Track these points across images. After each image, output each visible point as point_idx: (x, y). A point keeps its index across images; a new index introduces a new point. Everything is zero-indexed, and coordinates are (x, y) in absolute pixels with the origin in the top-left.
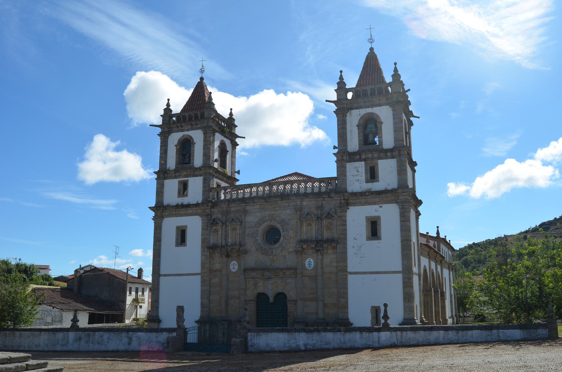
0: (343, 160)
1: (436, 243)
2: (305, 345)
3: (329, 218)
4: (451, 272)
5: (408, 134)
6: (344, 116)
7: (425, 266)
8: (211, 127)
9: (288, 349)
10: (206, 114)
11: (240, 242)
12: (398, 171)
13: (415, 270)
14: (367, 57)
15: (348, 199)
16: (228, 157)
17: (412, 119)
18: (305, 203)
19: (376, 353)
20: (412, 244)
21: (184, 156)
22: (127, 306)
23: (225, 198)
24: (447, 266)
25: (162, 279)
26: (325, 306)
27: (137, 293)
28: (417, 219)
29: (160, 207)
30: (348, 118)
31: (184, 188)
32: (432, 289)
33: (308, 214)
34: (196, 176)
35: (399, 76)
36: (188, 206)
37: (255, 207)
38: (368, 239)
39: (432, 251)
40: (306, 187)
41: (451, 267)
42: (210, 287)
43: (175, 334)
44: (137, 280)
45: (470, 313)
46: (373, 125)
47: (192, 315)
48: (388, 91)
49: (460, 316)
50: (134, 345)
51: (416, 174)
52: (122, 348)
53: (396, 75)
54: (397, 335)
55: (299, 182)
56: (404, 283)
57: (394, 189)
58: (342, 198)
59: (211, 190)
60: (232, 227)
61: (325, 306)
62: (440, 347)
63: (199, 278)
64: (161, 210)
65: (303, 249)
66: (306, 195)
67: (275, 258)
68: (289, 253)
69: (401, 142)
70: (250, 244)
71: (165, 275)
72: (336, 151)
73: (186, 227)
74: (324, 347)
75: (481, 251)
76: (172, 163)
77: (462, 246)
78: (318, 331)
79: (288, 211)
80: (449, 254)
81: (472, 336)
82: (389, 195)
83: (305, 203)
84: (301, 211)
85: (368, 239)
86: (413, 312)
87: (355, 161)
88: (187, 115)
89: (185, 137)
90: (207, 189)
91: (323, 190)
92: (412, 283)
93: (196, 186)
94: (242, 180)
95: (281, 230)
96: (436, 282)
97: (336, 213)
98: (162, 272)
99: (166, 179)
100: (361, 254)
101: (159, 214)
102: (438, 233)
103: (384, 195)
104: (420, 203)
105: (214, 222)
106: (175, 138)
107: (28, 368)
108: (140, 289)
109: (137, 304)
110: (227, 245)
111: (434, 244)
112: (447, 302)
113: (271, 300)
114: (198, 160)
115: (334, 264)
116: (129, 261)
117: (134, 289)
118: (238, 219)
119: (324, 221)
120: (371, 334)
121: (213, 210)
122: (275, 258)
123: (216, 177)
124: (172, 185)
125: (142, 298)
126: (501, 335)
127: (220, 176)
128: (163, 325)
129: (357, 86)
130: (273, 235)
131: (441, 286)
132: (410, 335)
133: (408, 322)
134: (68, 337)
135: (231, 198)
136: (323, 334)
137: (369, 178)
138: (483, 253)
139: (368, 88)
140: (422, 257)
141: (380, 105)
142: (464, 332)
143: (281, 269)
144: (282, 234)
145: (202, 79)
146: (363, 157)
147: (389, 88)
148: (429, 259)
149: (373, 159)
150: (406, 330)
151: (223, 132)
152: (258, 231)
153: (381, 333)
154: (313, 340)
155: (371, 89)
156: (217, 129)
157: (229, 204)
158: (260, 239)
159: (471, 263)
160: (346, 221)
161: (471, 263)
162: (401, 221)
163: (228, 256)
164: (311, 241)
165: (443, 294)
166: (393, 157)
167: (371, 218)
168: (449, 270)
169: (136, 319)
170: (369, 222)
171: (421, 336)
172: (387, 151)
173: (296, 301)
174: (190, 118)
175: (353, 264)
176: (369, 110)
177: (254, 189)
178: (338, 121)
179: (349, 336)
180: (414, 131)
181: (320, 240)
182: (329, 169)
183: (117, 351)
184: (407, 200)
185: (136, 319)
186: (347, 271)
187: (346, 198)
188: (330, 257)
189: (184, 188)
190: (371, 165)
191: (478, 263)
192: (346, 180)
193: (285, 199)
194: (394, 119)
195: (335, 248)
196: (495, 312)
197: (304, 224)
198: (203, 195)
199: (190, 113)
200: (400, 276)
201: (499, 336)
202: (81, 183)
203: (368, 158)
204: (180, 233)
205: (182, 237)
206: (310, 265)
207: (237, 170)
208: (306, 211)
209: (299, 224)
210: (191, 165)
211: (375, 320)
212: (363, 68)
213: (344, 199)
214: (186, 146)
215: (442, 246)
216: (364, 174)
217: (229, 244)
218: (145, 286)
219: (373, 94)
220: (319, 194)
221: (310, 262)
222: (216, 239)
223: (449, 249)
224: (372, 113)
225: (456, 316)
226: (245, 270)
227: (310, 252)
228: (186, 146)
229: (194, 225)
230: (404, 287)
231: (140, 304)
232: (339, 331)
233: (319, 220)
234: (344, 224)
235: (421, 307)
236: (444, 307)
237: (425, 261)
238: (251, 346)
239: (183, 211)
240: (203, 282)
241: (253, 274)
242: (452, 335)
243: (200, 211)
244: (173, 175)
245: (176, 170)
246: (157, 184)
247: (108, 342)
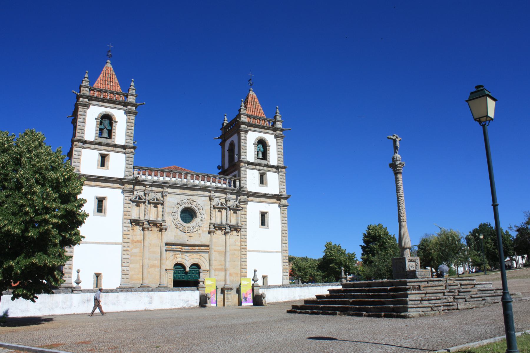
70: (169, 222)
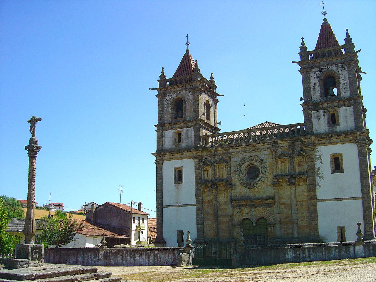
8: (197, 87)
14: (322, 26)
17: (360, 74)
26: (299, 227)
51: (366, 119)
53: (348, 40)
59: (201, 138)
60: (220, 167)
61: (299, 227)
64: (161, 154)
65: (279, 182)
70: (235, 179)
71: (192, 205)
72: (302, 102)
76: (168, 117)
94: (224, 129)
95: (260, 168)
100: (327, 184)
107: (84, 279)
108: (141, 218)
117: (136, 218)
123: (204, 128)
125: (142, 225)
130: (253, 173)
145: (187, 51)
158: (243, 176)
166: (349, 105)
173: (275, 224)
174: (181, 82)
180: (362, 83)
188: (301, 188)
195: (305, 181)
197: (279, 163)
199: (180, 78)
200: (360, 201)
205: (179, 176)
209: (274, 162)
222: (207, 175)
227: (284, 184)
229: (189, 166)
240: (198, 210)
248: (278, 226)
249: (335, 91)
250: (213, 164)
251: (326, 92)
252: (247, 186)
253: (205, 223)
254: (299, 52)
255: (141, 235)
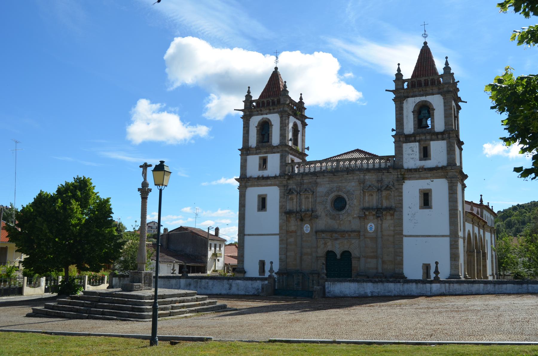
0: (400, 141)
1: (479, 209)
2: (372, 292)
3: (388, 190)
4: (493, 235)
5: (456, 117)
6: (402, 103)
7: (469, 231)
8: (286, 111)
9: (357, 295)
10: (282, 101)
11: (312, 208)
12: (447, 151)
13: (461, 234)
14: (422, 51)
15: (404, 174)
16: (300, 135)
18: (367, 177)
19: (430, 299)
20: (459, 212)
21: (263, 135)
22: (208, 259)
23: (299, 172)
24: (489, 229)
25: (247, 238)
26: (384, 262)
27: (215, 248)
28: (463, 190)
29: (244, 178)
30: (405, 105)
31: (264, 163)
32: (475, 250)
33: (370, 186)
34: (274, 153)
35: (450, 69)
36: (268, 178)
37: (324, 180)
38: (421, 208)
39: (475, 217)
40: (368, 163)
41: (492, 230)
42: (287, 245)
43: (266, 282)
44: (215, 238)
45: (510, 272)
46: (426, 111)
47: (276, 268)
48: (440, 81)
49: (500, 275)
50: (234, 290)
52: (224, 292)
53: (447, 68)
54: (445, 287)
55: (362, 159)
56: (451, 245)
57: (444, 166)
58: (399, 173)
60: (305, 196)
61: (384, 262)
62: (480, 296)
63: (277, 237)
64: (245, 181)
65: (366, 215)
66: (368, 170)
67: (342, 222)
68: (354, 218)
69: (450, 127)
70: (320, 210)
71: (249, 235)
72: (394, 133)
73: (266, 195)
74: (387, 294)
75: (525, 212)
76: (253, 142)
77: (507, 208)
78: (382, 282)
79: (353, 184)
80: (491, 219)
81: (506, 289)
82: (439, 171)
83: (367, 177)
84: (364, 184)
85: (421, 208)
86: (459, 269)
87: (410, 142)
88: (265, 101)
89: (264, 120)
90: (284, 164)
91: (383, 165)
92: (458, 245)
93: (274, 162)
95: (347, 200)
96: (479, 244)
97: (393, 186)
98: (246, 232)
99: (248, 155)
101: (243, 184)
102: (481, 201)
103: (435, 171)
104: (466, 177)
105: (290, 192)
106: (255, 120)
109: (215, 258)
110: (301, 211)
111: (478, 210)
112: (489, 262)
113: (338, 257)
114: (275, 140)
115: (392, 228)
116: (180, 217)
117: (213, 245)
118: (311, 190)
119: (384, 192)
120: (424, 285)
121: (289, 182)
122: (342, 222)
123: (291, 154)
124: (254, 160)
126: (530, 288)
127: (294, 153)
128: (247, 275)
129: (412, 76)
130: (339, 204)
131: (483, 247)
132: (456, 286)
133: (454, 277)
134: (180, 283)
135: (304, 172)
136: (386, 284)
137: (422, 157)
138: (528, 214)
139: (422, 79)
140: (466, 224)
141: (433, 94)
142: (500, 286)
143: (347, 232)
144: (348, 202)
146: (418, 138)
147: (441, 79)
148: (473, 224)
149: (426, 140)
150: (453, 282)
151: (295, 115)
152: (327, 199)
153: (430, 285)
154: (378, 289)
155: (425, 80)
156: (290, 113)
157: (302, 177)
158: (329, 206)
159: (515, 224)
160: (402, 193)
161: (515, 224)
162: (449, 193)
163: (302, 220)
164: (373, 209)
165: (484, 255)
167: (424, 190)
168: (491, 233)
169: (215, 271)
170: (422, 194)
171: (465, 287)
172: (438, 134)
173: (359, 258)
175: (407, 228)
176: (423, 98)
177: (324, 164)
178: (396, 108)
179: (407, 286)
181: (380, 209)
182: (389, 150)
183: (220, 294)
184: (455, 175)
185: (215, 271)
186: (402, 234)
187: (403, 173)
188: (388, 222)
189: (264, 163)
190: (425, 146)
191: (522, 225)
192: (402, 158)
193: (350, 174)
194: (445, 106)
195: (392, 215)
196: (526, 270)
198: (280, 169)
200: (448, 239)
201: (528, 289)
202: (129, 142)
203: (422, 140)
204: (261, 200)
206: (371, 228)
207: (306, 147)
208: (368, 183)
209: (362, 194)
210: (270, 143)
211: (426, 275)
212: (418, 61)
213: (401, 174)
214: (265, 128)
215: (485, 212)
216: (418, 154)
217: (303, 210)
218: (221, 243)
219: (426, 84)
220: (380, 170)
221: (371, 227)
222: (291, 206)
223: (491, 214)
224: (426, 101)
225: (496, 274)
226: (316, 232)
227: (371, 218)
228: (265, 128)
229: (273, 194)
230: (451, 249)
231: (218, 258)
232: (399, 282)
233: (379, 191)
234: (401, 195)
235: (464, 266)
236: (485, 266)
237: (469, 226)
238: (328, 292)
239: (263, 182)
240: (281, 241)
241: (323, 235)
242: (490, 287)
243: (278, 182)
244: (255, 152)
245: (257, 148)
246: (241, 159)
247: (212, 288)
248: (363, 260)
249: (429, 122)
250: (298, 193)
251: (420, 123)
252: (333, 218)
253: (288, 254)
254: (394, 79)
255: (218, 263)
